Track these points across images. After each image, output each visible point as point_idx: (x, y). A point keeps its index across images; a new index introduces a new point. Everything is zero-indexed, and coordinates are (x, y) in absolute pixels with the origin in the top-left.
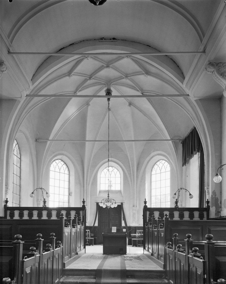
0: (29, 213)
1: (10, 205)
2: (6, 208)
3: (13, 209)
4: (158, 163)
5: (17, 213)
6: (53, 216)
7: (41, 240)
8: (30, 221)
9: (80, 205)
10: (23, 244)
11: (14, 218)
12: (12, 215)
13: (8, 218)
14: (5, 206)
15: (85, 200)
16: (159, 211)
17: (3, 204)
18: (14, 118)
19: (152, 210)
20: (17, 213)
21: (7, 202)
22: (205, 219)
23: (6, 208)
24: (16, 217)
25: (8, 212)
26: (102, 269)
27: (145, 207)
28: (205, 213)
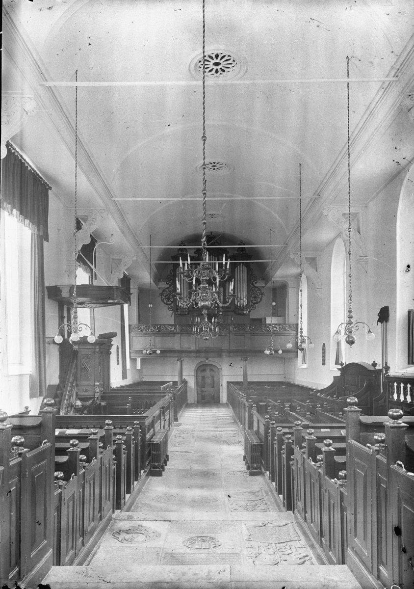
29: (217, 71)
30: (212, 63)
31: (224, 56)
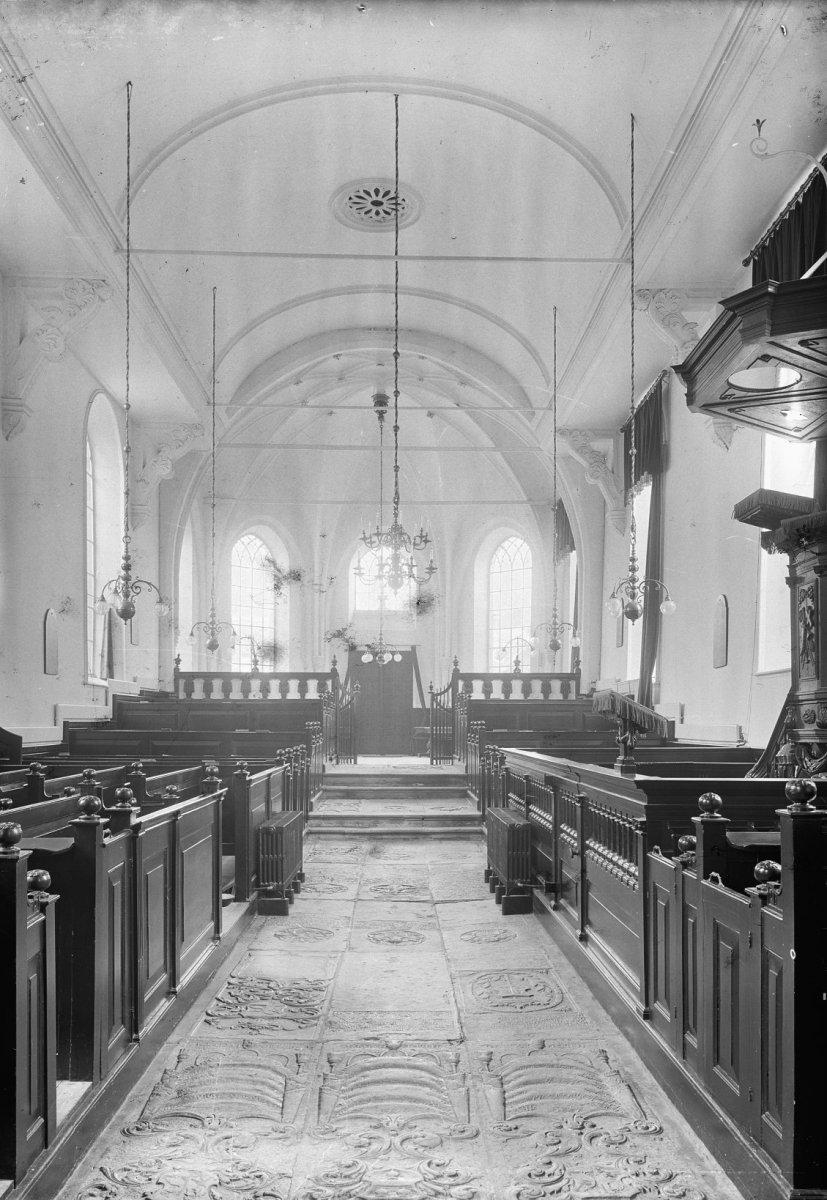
0: (562, 686)
1: (184, 668)
2: (178, 675)
3: (191, 677)
4: (506, 544)
5: (478, 685)
6: (196, 692)
7: (99, 824)
8: (283, 705)
9: (327, 669)
10: (58, 903)
11: (492, 696)
12: (189, 690)
13: (182, 696)
14: (176, 670)
15: (337, 659)
16: (502, 679)
17: (174, 665)
18: (88, 627)
19: (469, 678)
20: (198, 685)
21: (178, 661)
22: (572, 696)
23: (178, 675)
24: (198, 694)
25: (182, 682)
26: (121, 6)
27: (456, 671)
28: (573, 684)
29: (377, 213)
30: (370, 200)
31: (366, 213)
